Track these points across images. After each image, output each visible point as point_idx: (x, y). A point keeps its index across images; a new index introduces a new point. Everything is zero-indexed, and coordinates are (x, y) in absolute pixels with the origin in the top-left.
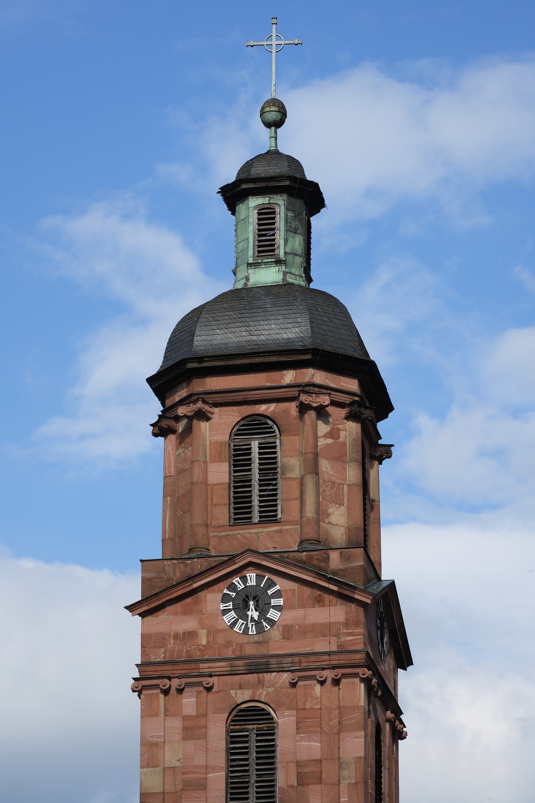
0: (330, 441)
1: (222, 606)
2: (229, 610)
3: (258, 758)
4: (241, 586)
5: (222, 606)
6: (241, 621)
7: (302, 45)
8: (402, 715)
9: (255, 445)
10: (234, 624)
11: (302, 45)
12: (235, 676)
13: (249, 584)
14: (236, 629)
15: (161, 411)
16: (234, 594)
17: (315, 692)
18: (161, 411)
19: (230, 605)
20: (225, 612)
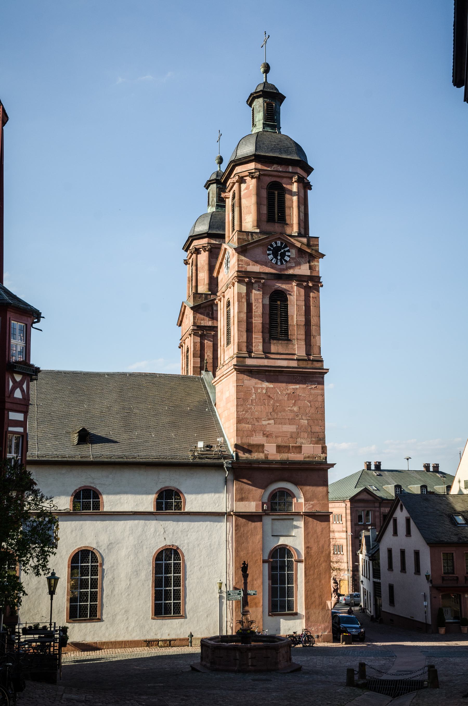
0: (246, 191)
1: (268, 252)
2: (270, 254)
3: (277, 319)
4: (275, 246)
5: (268, 252)
6: (274, 259)
7: (410, 458)
8: (68, 630)
9: (276, 192)
10: (272, 260)
11: (410, 458)
12: (201, 510)
13: (278, 245)
14: (273, 261)
15: (285, 97)
16: (272, 248)
17: (248, 611)
18: (285, 97)
19: (271, 252)
20: (269, 255)
